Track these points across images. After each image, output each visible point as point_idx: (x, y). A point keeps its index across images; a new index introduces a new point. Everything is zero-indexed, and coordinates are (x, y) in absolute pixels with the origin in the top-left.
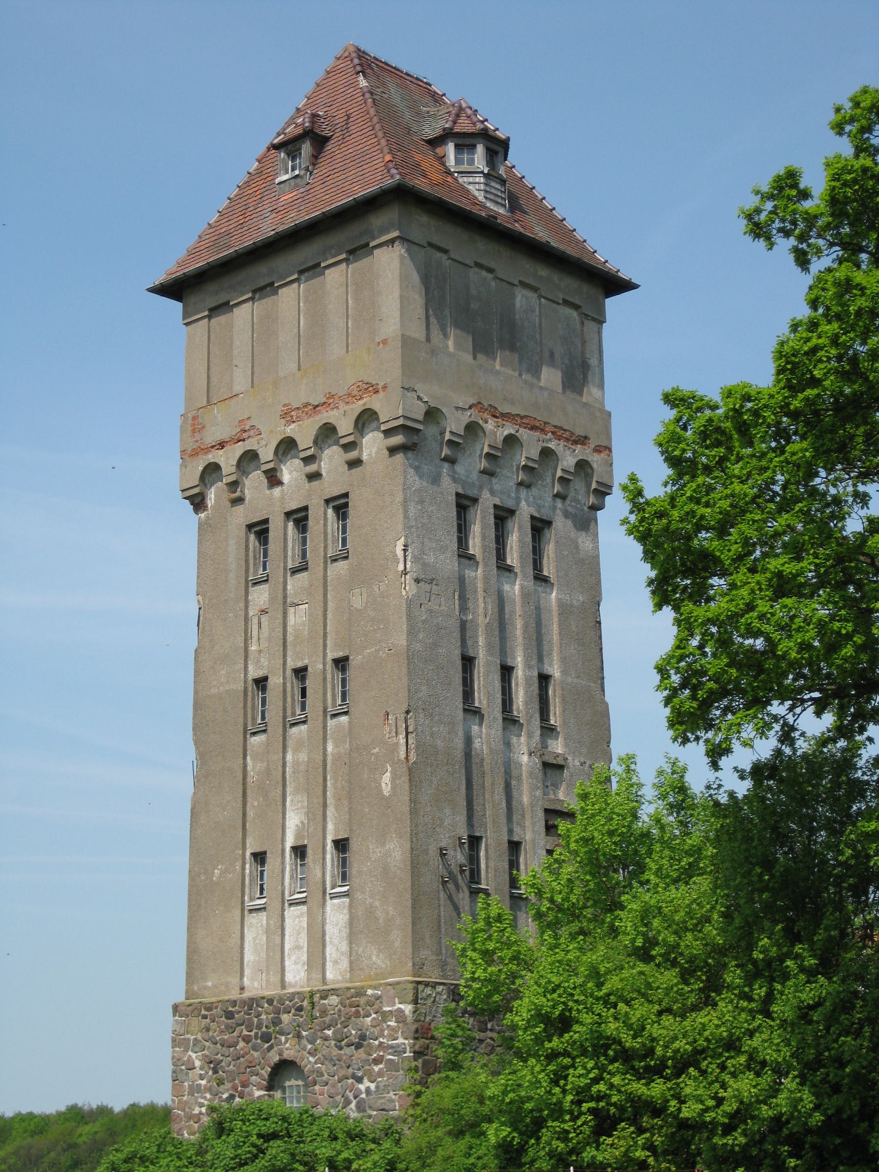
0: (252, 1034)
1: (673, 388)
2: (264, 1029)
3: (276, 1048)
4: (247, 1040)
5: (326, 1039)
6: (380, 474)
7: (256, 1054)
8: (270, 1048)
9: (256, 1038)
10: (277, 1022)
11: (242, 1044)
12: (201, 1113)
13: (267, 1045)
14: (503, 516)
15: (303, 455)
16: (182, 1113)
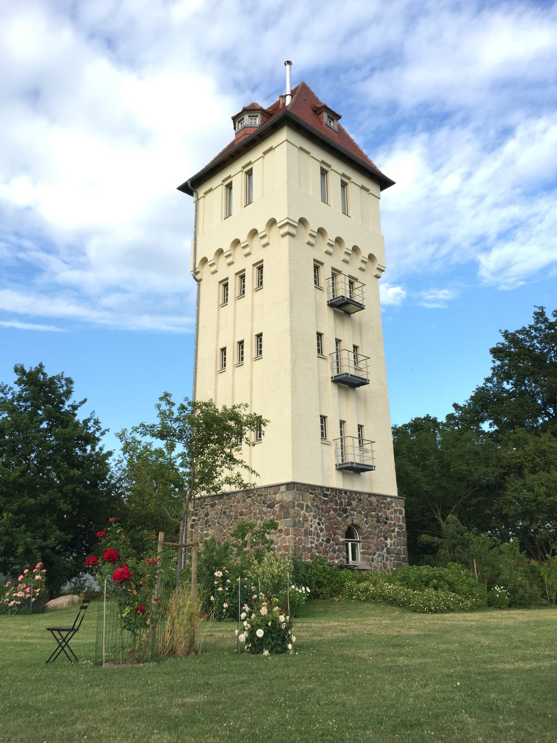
0: (338, 507)
1: (496, 352)
2: (343, 507)
3: (350, 518)
4: (335, 510)
5: (372, 517)
6: (278, 254)
7: (340, 519)
8: (347, 517)
9: (340, 510)
10: (349, 504)
11: (332, 512)
12: (312, 547)
13: (345, 515)
14: (335, 273)
15: (243, 245)
16: (14, 602)
